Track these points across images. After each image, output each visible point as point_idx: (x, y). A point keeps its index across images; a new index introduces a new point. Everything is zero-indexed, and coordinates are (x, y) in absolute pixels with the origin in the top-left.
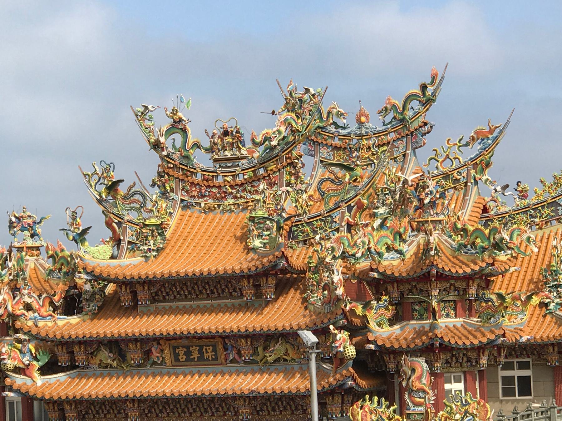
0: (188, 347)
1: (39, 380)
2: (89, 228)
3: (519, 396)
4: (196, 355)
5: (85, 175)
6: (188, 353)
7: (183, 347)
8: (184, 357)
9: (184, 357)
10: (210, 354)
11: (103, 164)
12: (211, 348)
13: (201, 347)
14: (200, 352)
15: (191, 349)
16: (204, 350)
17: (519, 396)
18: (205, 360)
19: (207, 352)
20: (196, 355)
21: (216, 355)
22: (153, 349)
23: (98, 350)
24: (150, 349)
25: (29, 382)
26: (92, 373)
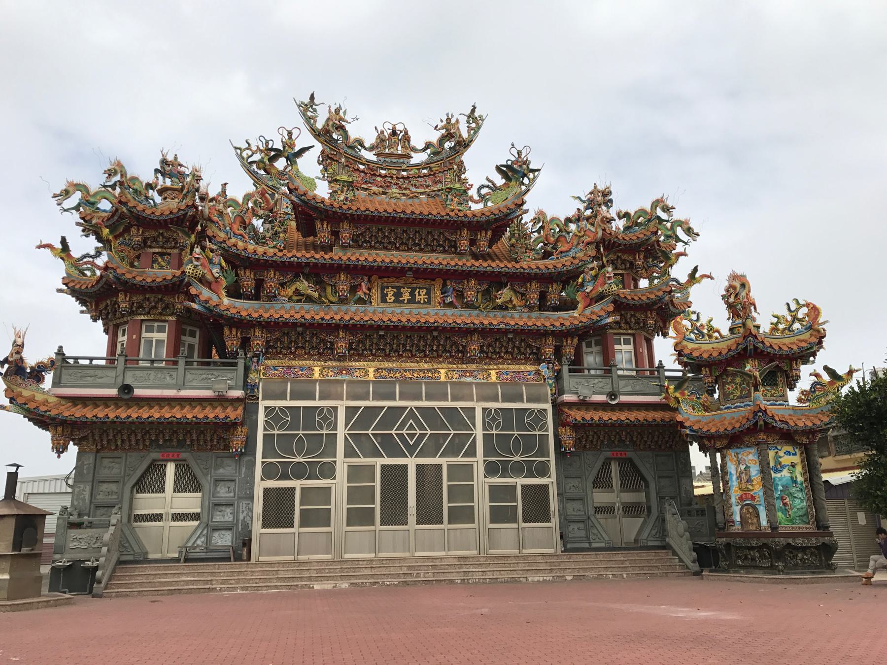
0: (399, 289)
1: (226, 301)
2: (313, 146)
3: (267, 491)
4: (406, 296)
5: (236, 148)
6: (398, 295)
7: (393, 288)
8: (393, 298)
9: (393, 298)
10: (422, 297)
11: (262, 139)
12: (425, 291)
13: (413, 290)
14: (412, 294)
15: (402, 290)
16: (417, 293)
17: (267, 491)
18: (415, 303)
19: (419, 295)
20: (406, 296)
21: (429, 299)
22: (363, 284)
23: (297, 276)
24: (360, 285)
25: (215, 298)
26: (280, 306)
